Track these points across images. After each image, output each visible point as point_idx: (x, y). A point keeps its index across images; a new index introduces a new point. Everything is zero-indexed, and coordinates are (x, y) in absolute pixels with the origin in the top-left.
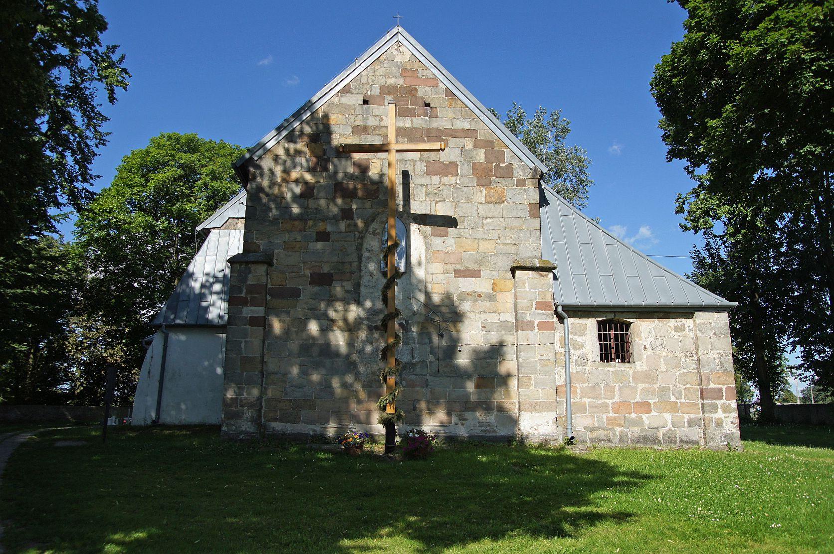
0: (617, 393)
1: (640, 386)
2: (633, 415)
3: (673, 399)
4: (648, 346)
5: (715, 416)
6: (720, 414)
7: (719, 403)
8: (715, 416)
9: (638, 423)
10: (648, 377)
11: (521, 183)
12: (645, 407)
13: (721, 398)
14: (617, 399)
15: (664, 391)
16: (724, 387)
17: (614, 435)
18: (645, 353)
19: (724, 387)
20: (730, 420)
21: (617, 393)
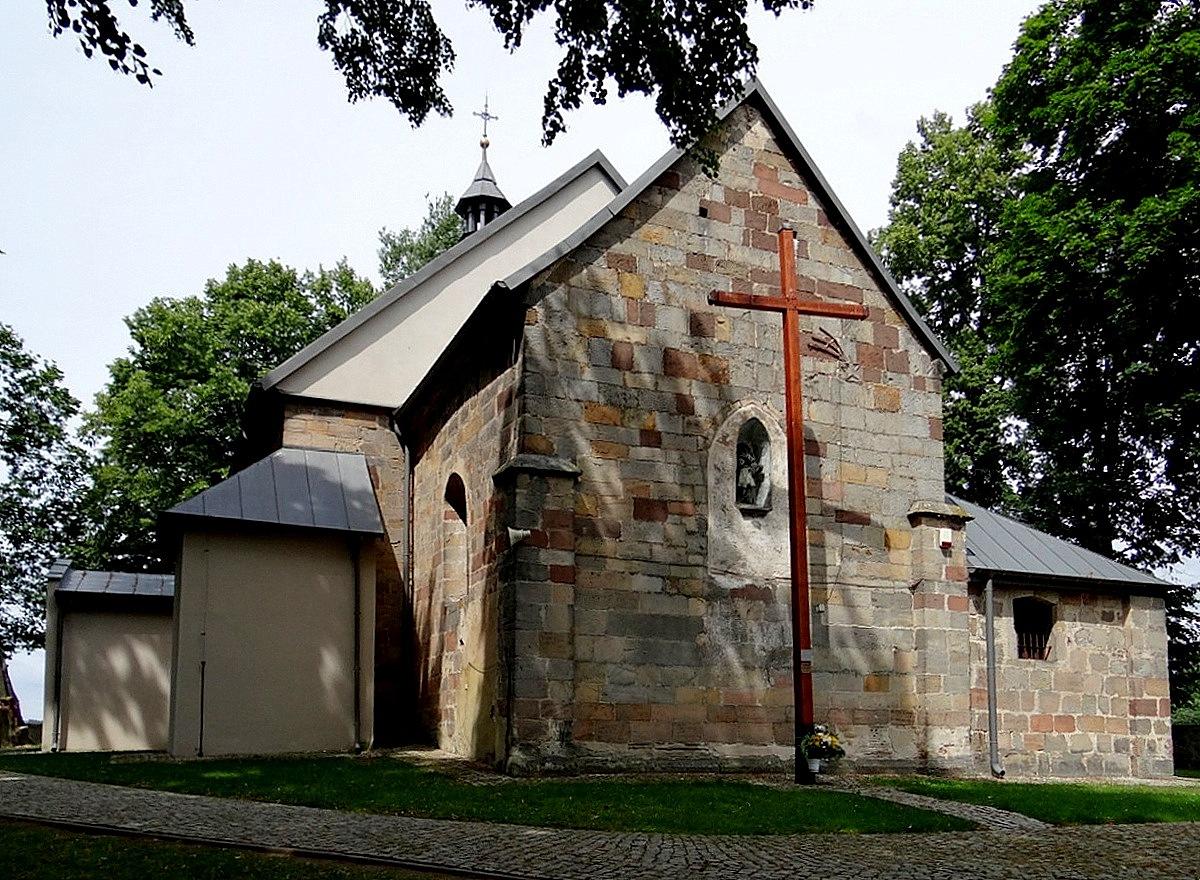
0: (1036, 702)
1: (1063, 694)
2: (1055, 734)
3: (1099, 713)
5: (1147, 737)
6: (1153, 735)
7: (1153, 719)
8: (1147, 737)
10: (1074, 682)
12: (1067, 723)
14: (1035, 712)
16: (1158, 699)
17: (1034, 761)
18: (1069, 649)
19: (1158, 699)
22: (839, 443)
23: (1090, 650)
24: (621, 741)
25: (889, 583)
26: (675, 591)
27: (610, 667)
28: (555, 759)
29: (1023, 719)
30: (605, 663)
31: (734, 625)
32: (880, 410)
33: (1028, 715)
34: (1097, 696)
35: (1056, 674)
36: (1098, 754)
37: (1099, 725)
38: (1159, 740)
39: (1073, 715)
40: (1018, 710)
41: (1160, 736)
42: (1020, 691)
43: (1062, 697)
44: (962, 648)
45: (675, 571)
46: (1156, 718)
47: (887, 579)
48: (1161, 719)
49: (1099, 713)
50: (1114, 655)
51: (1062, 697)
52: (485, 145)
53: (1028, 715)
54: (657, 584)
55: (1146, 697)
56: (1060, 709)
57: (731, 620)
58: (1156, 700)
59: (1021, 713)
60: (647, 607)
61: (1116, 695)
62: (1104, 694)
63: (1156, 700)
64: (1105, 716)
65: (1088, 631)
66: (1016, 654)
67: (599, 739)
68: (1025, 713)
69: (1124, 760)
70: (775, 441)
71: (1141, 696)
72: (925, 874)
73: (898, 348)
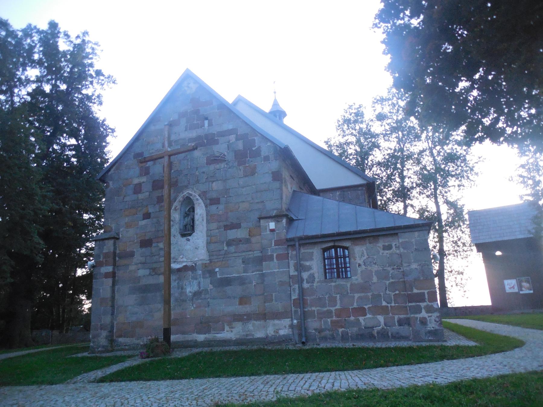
0: (338, 302)
1: (357, 296)
2: (352, 318)
3: (384, 304)
4: (362, 263)
6: (424, 314)
7: (423, 305)
9: (358, 322)
10: (364, 288)
12: (361, 311)
13: (423, 300)
14: (338, 307)
15: (376, 298)
16: (426, 292)
18: (359, 270)
19: (426, 292)
20: (433, 318)
21: (338, 302)
22: (226, 196)
24: (132, 337)
25: (250, 253)
26: (154, 273)
27: (130, 307)
28: (103, 347)
29: (330, 312)
30: (128, 306)
31: (178, 283)
32: (246, 176)
33: (333, 309)
34: (382, 294)
35: (352, 285)
36: (385, 328)
37: (384, 311)
38: (429, 317)
39: (365, 306)
40: (326, 307)
41: (430, 314)
42: (327, 297)
43: (356, 298)
44: (285, 278)
45: (155, 266)
46: (425, 304)
47: (251, 251)
48: (430, 304)
49: (384, 304)
50: (393, 269)
51: (356, 298)
52: (275, 93)
53: (333, 309)
54: (147, 272)
55: (415, 291)
56: (355, 304)
57: (177, 282)
58: (424, 293)
59: (328, 308)
60: (144, 282)
61: (397, 292)
62: (388, 292)
63: (424, 293)
64: (389, 305)
65: (373, 258)
67: (124, 337)
68: (331, 308)
69: (405, 330)
70: (196, 204)
71: (412, 290)
72: (81, 379)
73: (255, 147)
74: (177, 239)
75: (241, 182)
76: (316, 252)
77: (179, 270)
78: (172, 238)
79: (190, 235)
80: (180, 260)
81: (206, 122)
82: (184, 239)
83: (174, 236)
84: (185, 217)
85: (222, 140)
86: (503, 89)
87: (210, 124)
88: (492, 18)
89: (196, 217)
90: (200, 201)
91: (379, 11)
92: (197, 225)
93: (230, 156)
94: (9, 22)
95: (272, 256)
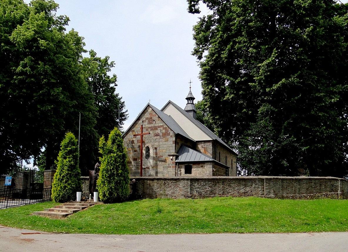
11: (171, 136)
23: (198, 172)
32: (165, 141)
66: (184, 173)
74: (144, 159)
75: (164, 143)
76: (183, 166)
77: (145, 168)
78: (143, 159)
79: (148, 158)
80: (145, 165)
81: (154, 122)
82: (147, 159)
83: (144, 158)
84: (147, 152)
85: (159, 129)
86: (275, 131)
87: (155, 123)
88: (336, 108)
89: (150, 153)
90: (151, 148)
91: (105, 64)
92: (163, 176)
93: (161, 134)
94: (193, 14)
95: (171, 166)
